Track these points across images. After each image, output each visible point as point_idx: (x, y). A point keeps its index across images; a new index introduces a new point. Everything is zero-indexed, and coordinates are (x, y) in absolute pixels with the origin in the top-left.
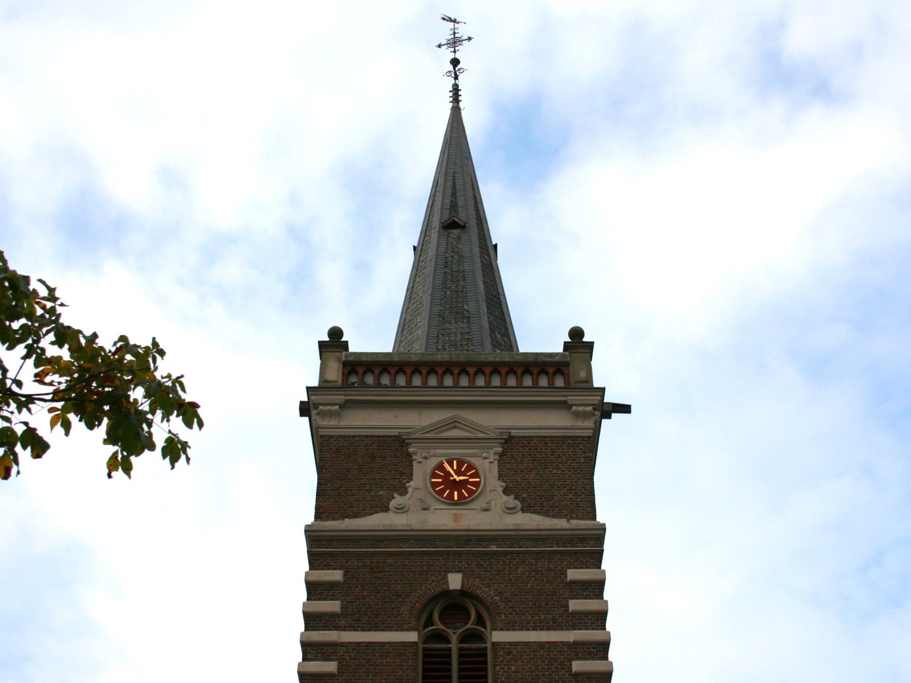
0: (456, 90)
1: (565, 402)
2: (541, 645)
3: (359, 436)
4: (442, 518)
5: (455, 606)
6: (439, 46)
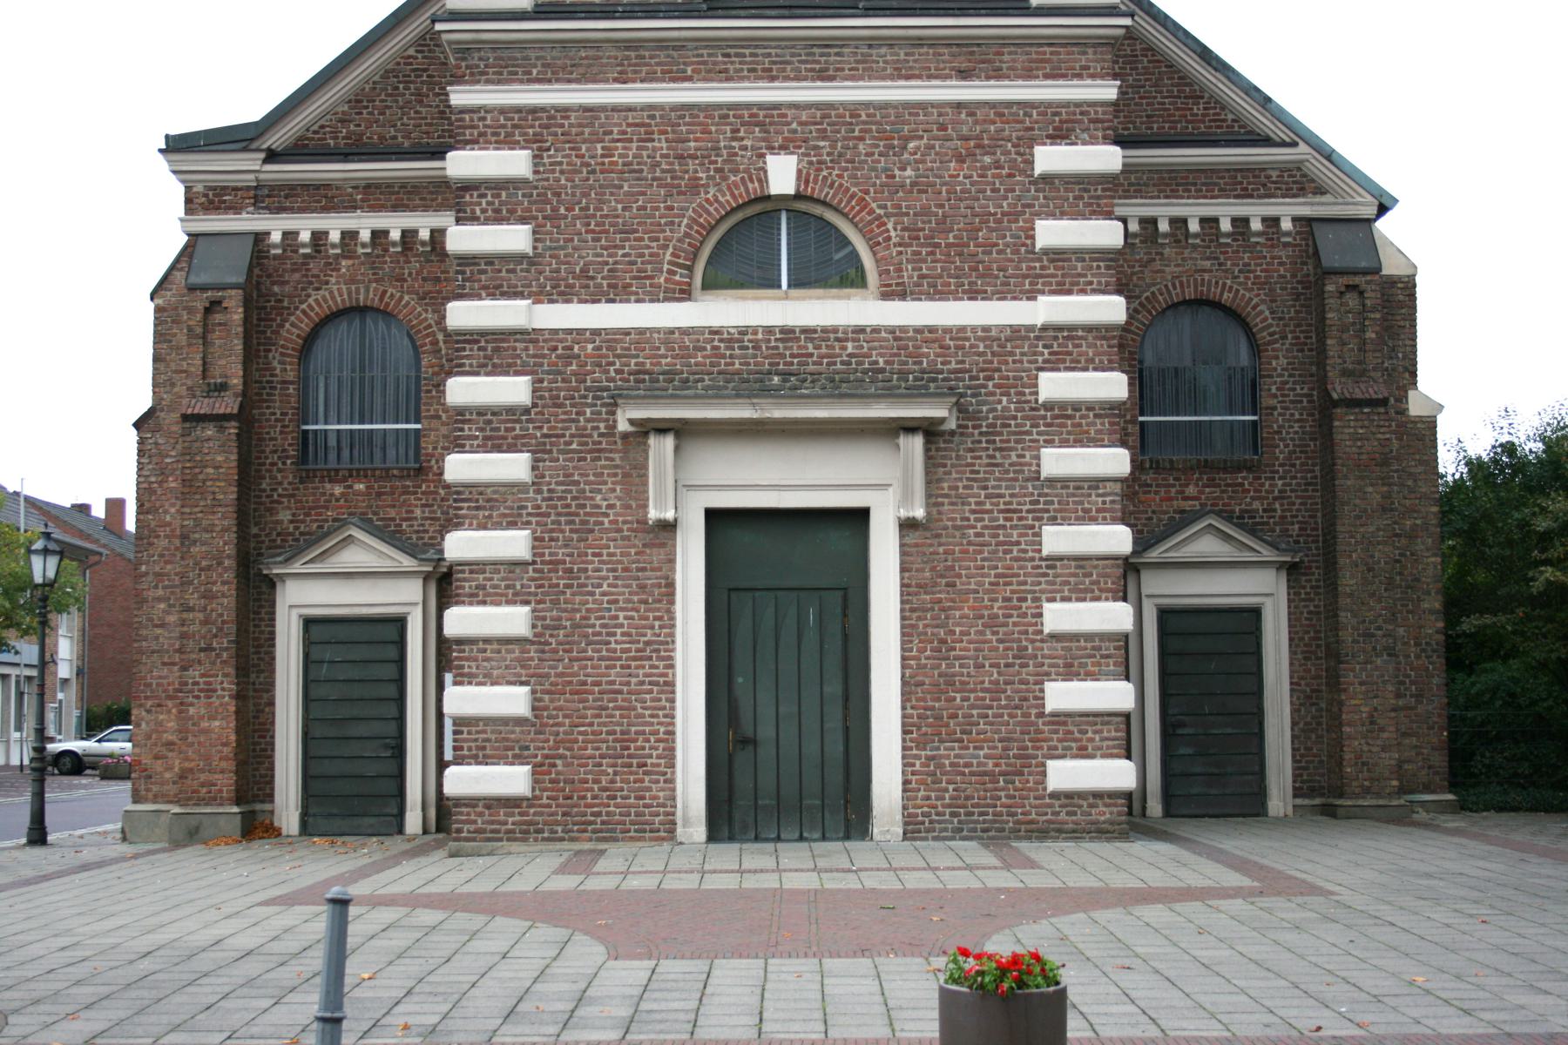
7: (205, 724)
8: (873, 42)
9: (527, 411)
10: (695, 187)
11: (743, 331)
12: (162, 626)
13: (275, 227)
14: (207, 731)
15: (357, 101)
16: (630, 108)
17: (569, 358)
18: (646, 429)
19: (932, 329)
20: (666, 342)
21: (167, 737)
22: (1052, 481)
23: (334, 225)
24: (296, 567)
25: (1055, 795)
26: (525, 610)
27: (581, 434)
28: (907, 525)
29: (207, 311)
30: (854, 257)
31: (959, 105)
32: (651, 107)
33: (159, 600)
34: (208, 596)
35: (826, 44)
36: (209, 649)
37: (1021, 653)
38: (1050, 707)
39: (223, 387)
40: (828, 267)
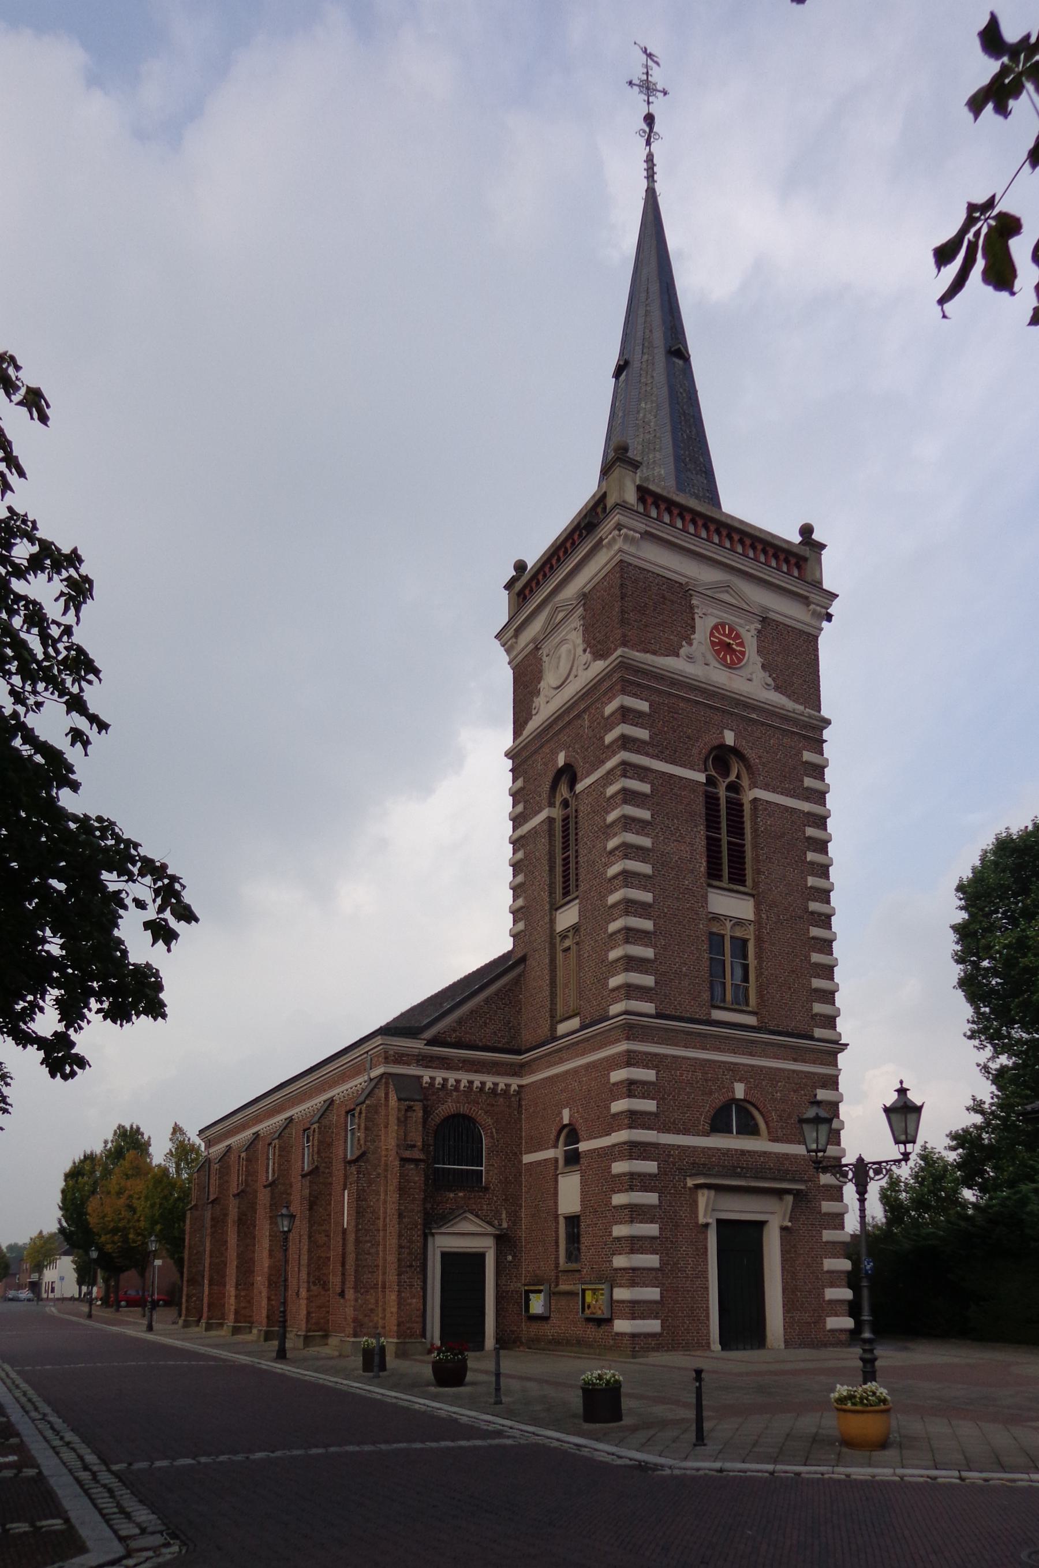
0: (650, 159)
1: (807, 598)
2: (787, 809)
3: (653, 573)
4: (719, 676)
5: (721, 758)
6: (944, 316)
7: (409, 1301)
8: (767, 1044)
9: (655, 1176)
10: (711, 1093)
11: (728, 1150)
12: (369, 1254)
13: (427, 1075)
14: (410, 1304)
15: (460, 1022)
16: (689, 1058)
17: (669, 1156)
18: (698, 1187)
19: (787, 1155)
20: (703, 1152)
21: (371, 1306)
22: (825, 1214)
23: (452, 1077)
24: (443, 1230)
25: (830, 1331)
26: (658, 1256)
27: (674, 1187)
28: (783, 1229)
29: (406, 1111)
30: (756, 1125)
31: (794, 1071)
32: (696, 1059)
33: (367, 1242)
34: (411, 1241)
35: (753, 1042)
36: (411, 1266)
37: (817, 1278)
38: (827, 1298)
39: (414, 1146)
40: (749, 1129)
